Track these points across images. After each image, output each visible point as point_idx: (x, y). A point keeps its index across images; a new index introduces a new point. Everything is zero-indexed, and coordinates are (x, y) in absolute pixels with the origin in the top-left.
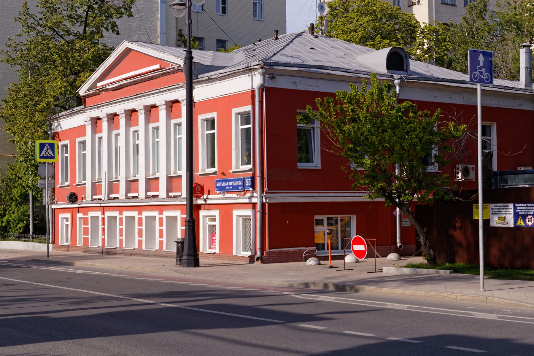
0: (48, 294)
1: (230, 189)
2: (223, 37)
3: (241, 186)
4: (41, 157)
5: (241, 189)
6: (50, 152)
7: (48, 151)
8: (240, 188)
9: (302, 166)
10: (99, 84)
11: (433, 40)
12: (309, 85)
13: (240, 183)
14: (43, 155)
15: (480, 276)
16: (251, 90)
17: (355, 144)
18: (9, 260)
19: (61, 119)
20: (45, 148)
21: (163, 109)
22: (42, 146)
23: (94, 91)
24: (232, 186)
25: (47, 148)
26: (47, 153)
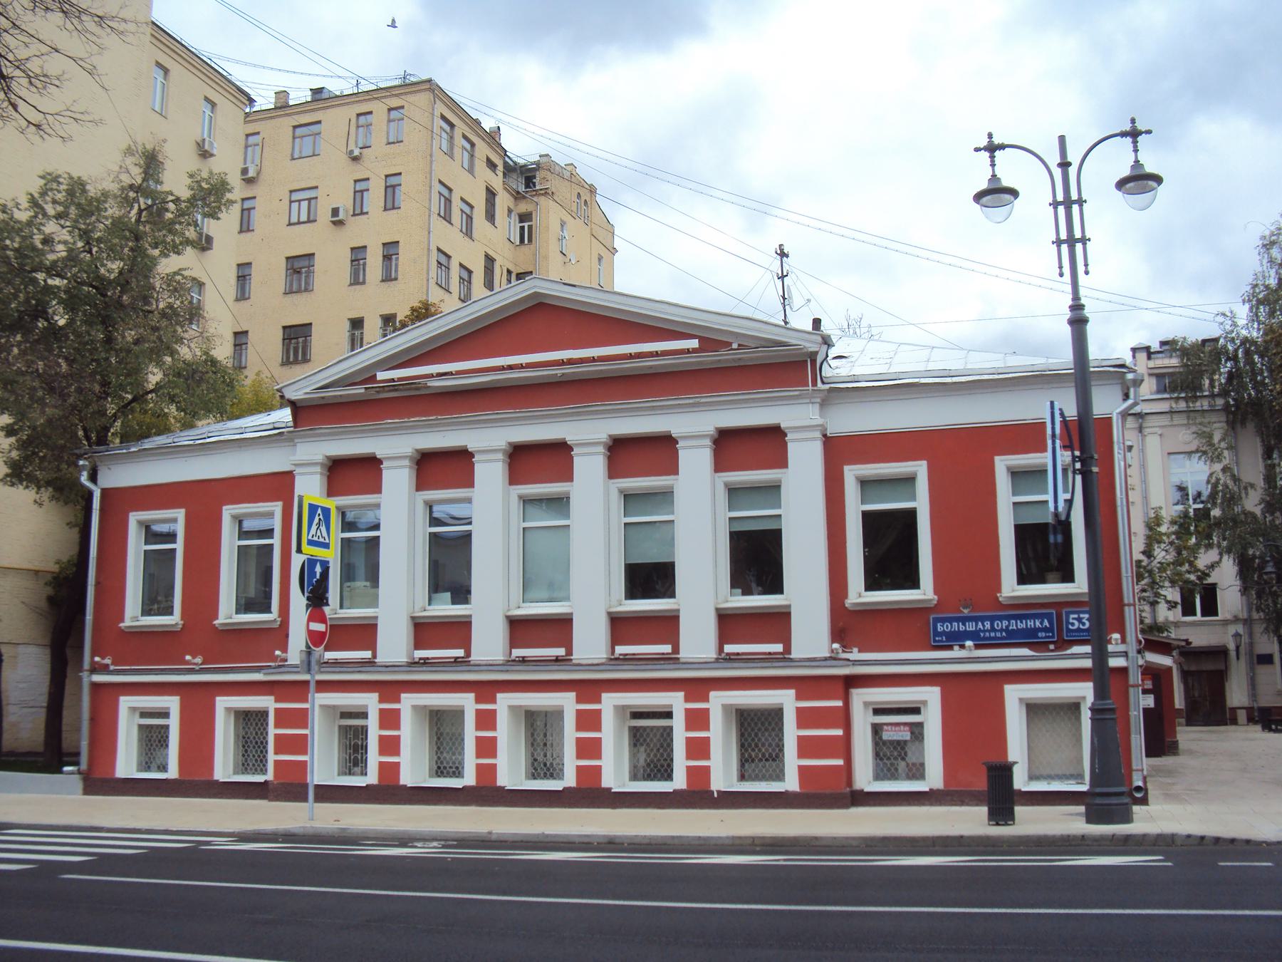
3: (1045, 630)
5: (1046, 637)
7: (321, 527)
10: (381, 376)
13: (1041, 623)
23: (363, 391)
24: (1007, 630)
25: (320, 519)
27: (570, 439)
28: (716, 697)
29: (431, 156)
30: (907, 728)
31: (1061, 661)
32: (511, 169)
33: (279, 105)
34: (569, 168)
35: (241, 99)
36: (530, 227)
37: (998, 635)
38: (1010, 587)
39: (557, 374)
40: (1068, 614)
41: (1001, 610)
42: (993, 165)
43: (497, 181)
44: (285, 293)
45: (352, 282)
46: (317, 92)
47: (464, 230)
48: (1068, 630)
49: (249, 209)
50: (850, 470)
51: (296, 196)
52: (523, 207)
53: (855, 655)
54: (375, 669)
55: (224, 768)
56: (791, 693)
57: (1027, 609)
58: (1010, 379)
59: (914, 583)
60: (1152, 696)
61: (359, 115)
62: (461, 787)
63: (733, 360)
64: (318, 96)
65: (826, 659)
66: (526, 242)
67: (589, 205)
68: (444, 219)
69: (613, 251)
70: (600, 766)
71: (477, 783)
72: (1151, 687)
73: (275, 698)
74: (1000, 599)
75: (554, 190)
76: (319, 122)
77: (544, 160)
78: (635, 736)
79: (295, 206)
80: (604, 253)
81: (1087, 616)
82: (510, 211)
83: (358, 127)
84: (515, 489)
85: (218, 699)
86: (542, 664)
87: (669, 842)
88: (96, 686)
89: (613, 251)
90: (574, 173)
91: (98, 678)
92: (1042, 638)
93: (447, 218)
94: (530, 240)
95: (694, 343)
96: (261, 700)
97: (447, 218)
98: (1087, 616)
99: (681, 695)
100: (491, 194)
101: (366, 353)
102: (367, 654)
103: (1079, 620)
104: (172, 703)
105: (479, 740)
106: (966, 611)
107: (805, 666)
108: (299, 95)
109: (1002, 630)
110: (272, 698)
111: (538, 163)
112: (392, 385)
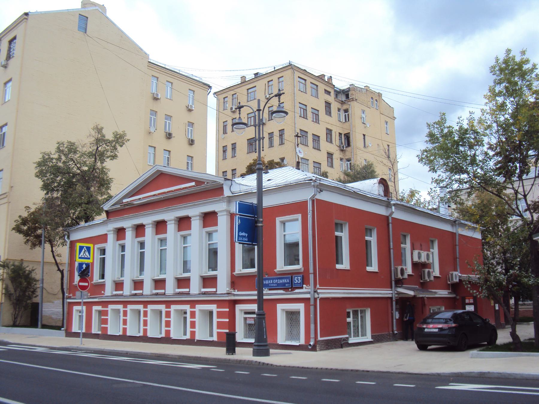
1: (274, 286)
3: (288, 283)
4: (80, 258)
5: (288, 286)
6: (87, 253)
8: (287, 285)
9: (338, 267)
11: (468, 150)
13: (287, 281)
16: (316, 189)
18: (499, 378)
19: (109, 222)
20: (83, 250)
21: (129, 231)
22: (81, 248)
23: (120, 206)
24: (277, 283)
25: (85, 250)
26: (84, 255)
27: (144, 223)
29: (294, 94)
30: (253, 319)
32: (338, 93)
33: (242, 82)
34: (366, 88)
35: (206, 87)
36: (348, 114)
37: (274, 285)
40: (295, 277)
41: (276, 276)
43: (331, 99)
44: (248, 153)
45: (280, 144)
46: (256, 74)
47: (315, 120)
48: (295, 284)
49: (226, 126)
51: (250, 116)
52: (345, 107)
53: (236, 292)
54: (190, 296)
55: (95, 330)
56: (215, 306)
60: (473, 306)
61: (268, 82)
62: (185, 339)
63: (204, 188)
64: (257, 76)
65: (225, 294)
66: (347, 121)
67: (378, 102)
68: (304, 118)
69: (393, 118)
70: (170, 330)
71: (254, 338)
72: (472, 302)
73: (123, 306)
75: (357, 98)
76: (255, 87)
77: (352, 86)
79: (249, 119)
80: (388, 120)
81: (300, 278)
82: (339, 110)
83: (269, 86)
85: (278, 305)
87: (139, 354)
88: (69, 303)
89: (393, 118)
90: (368, 89)
91: (69, 300)
92: (287, 286)
93: (305, 117)
94: (348, 120)
97: (305, 117)
98: (300, 278)
99: (189, 306)
100: (328, 105)
102: (214, 290)
103: (298, 279)
104: (300, 307)
105: (166, 321)
106: (266, 276)
107: (218, 296)
108: (250, 76)
109: (275, 283)
110: (101, 307)
111: (349, 88)
112: (128, 204)
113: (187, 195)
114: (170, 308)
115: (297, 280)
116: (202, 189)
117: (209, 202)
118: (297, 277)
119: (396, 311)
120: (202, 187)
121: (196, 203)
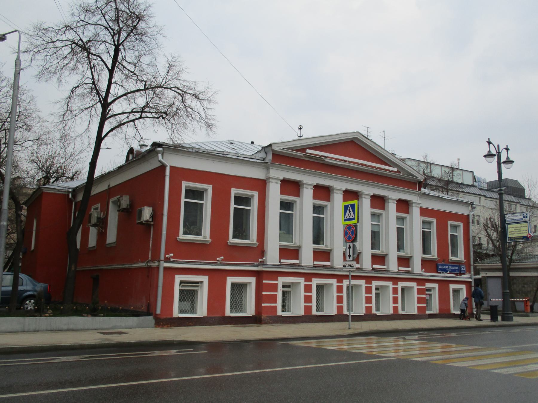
0: (226, 147)
2: (252, 144)
3: (458, 270)
5: (458, 272)
8: (457, 271)
10: (308, 151)
12: (206, 78)
14: (347, 217)
15: (313, 204)
17: (117, 17)
23: (302, 155)
28: (400, 284)
31: (196, 265)
38: (232, 240)
39: (362, 169)
42: (507, 154)
50: (233, 190)
57: (453, 264)
58: (452, 200)
59: (234, 237)
74: (178, 239)
78: (182, 293)
84: (185, 183)
86: (318, 269)
95: (396, 170)
96: (248, 279)
101: (401, 162)
104: (463, 287)
113: (383, 176)
114: (397, 284)
115: (463, 268)
116: (292, 154)
117: (352, 181)
118: (463, 266)
119: (425, 285)
120: (402, 175)
121: (398, 189)
